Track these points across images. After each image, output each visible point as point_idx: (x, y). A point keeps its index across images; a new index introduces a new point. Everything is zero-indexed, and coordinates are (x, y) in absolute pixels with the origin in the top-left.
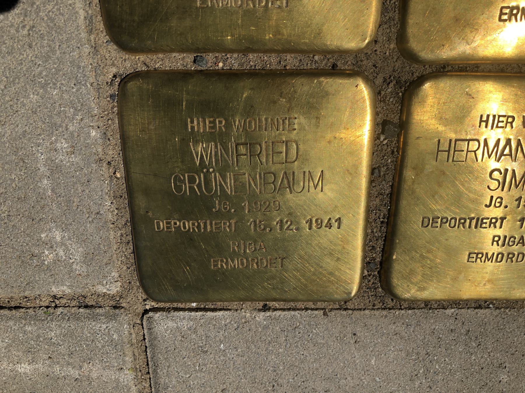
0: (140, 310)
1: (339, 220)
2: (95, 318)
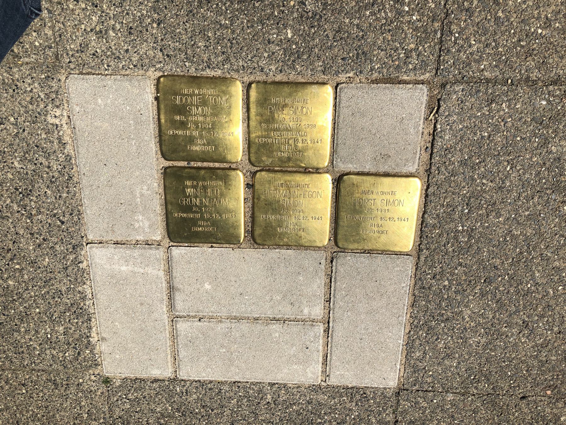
0: (167, 246)
1: (232, 133)
2: (151, 249)
